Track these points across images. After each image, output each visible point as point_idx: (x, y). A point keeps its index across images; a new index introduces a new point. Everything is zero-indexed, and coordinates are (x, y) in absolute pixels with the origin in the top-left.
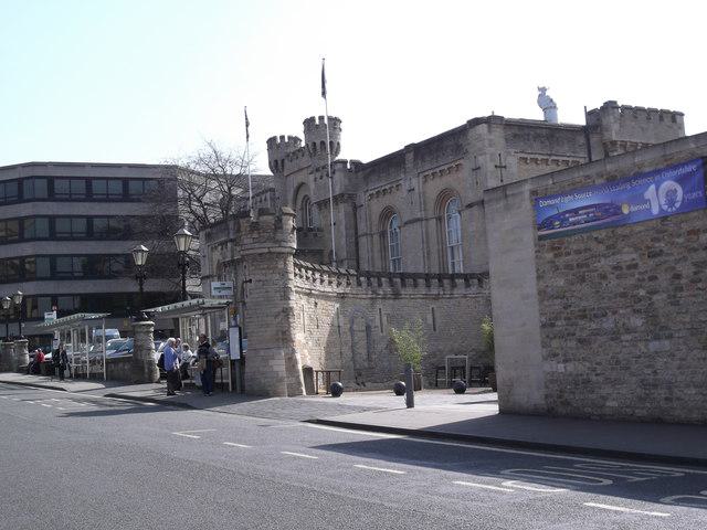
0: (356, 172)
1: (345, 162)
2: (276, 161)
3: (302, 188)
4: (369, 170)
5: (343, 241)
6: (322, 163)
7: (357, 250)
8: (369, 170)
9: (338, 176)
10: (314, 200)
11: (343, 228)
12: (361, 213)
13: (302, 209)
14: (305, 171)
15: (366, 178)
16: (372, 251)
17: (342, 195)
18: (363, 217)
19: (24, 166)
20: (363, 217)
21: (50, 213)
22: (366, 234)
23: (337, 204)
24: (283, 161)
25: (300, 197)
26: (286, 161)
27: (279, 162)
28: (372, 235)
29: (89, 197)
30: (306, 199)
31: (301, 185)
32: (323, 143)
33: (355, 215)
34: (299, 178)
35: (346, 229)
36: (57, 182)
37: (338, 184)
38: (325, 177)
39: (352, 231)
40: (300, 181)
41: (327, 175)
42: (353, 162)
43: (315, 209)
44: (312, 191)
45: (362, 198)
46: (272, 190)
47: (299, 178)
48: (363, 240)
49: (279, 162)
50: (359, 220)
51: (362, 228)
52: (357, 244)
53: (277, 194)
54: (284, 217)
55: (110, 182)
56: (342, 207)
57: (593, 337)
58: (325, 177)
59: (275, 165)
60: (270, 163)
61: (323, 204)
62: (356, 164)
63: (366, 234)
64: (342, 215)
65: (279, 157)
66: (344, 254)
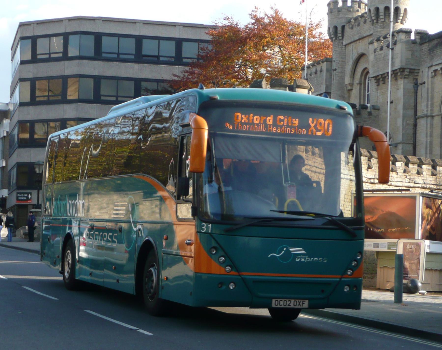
0: (421, 44)
1: (408, 32)
2: (336, 28)
3: (362, 60)
4: (435, 42)
5: (400, 122)
6: (384, 33)
7: (415, 134)
8: (435, 42)
9: (398, 47)
10: (372, 74)
11: (400, 107)
12: (423, 91)
13: (360, 84)
14: (366, 41)
15: (431, 51)
16: (431, 136)
17: (402, 70)
18: (424, 95)
19: (39, 23)
20: (424, 95)
21: (96, 73)
22: (427, 116)
23: (396, 80)
24: (343, 27)
25: (359, 70)
26: (347, 29)
27: (339, 29)
28: (433, 117)
29: (140, 57)
30: (365, 72)
31: (362, 56)
32: (387, 9)
33: (416, 92)
34: (361, 47)
35: (404, 108)
36: (105, 40)
37: (396, 58)
38: (385, 48)
39: (411, 112)
40: (361, 51)
41: (388, 46)
42: (418, 33)
43: (373, 84)
44: (371, 65)
45: (425, 75)
46: (329, 60)
47: (361, 47)
48: (422, 123)
49: (339, 29)
50: (419, 100)
51: (422, 109)
52: (415, 126)
53: (334, 66)
54: (362, 4)
55: (161, 42)
56: (401, 83)
57: (351, 26)
58: (385, 48)
59: (336, 32)
60: (329, 29)
61: (381, 79)
62: (423, 36)
63: (427, 116)
64: (400, 93)
65: (339, 23)
66: (399, 138)
